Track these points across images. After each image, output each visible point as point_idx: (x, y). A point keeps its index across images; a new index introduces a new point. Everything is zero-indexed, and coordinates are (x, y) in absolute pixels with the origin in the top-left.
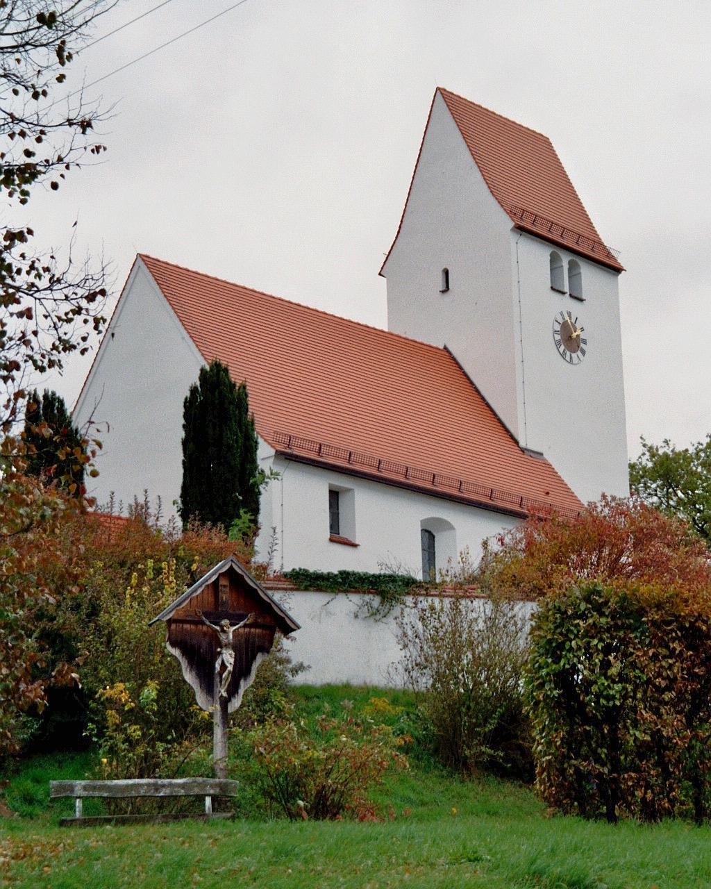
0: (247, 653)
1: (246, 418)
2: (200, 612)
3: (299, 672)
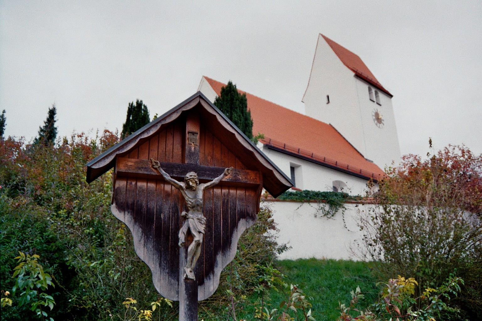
0: (225, 219)
1: (246, 110)
2: (156, 163)
3: (284, 251)
